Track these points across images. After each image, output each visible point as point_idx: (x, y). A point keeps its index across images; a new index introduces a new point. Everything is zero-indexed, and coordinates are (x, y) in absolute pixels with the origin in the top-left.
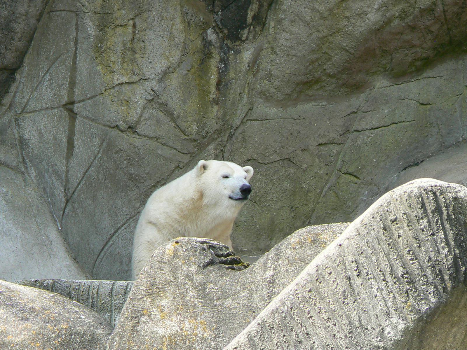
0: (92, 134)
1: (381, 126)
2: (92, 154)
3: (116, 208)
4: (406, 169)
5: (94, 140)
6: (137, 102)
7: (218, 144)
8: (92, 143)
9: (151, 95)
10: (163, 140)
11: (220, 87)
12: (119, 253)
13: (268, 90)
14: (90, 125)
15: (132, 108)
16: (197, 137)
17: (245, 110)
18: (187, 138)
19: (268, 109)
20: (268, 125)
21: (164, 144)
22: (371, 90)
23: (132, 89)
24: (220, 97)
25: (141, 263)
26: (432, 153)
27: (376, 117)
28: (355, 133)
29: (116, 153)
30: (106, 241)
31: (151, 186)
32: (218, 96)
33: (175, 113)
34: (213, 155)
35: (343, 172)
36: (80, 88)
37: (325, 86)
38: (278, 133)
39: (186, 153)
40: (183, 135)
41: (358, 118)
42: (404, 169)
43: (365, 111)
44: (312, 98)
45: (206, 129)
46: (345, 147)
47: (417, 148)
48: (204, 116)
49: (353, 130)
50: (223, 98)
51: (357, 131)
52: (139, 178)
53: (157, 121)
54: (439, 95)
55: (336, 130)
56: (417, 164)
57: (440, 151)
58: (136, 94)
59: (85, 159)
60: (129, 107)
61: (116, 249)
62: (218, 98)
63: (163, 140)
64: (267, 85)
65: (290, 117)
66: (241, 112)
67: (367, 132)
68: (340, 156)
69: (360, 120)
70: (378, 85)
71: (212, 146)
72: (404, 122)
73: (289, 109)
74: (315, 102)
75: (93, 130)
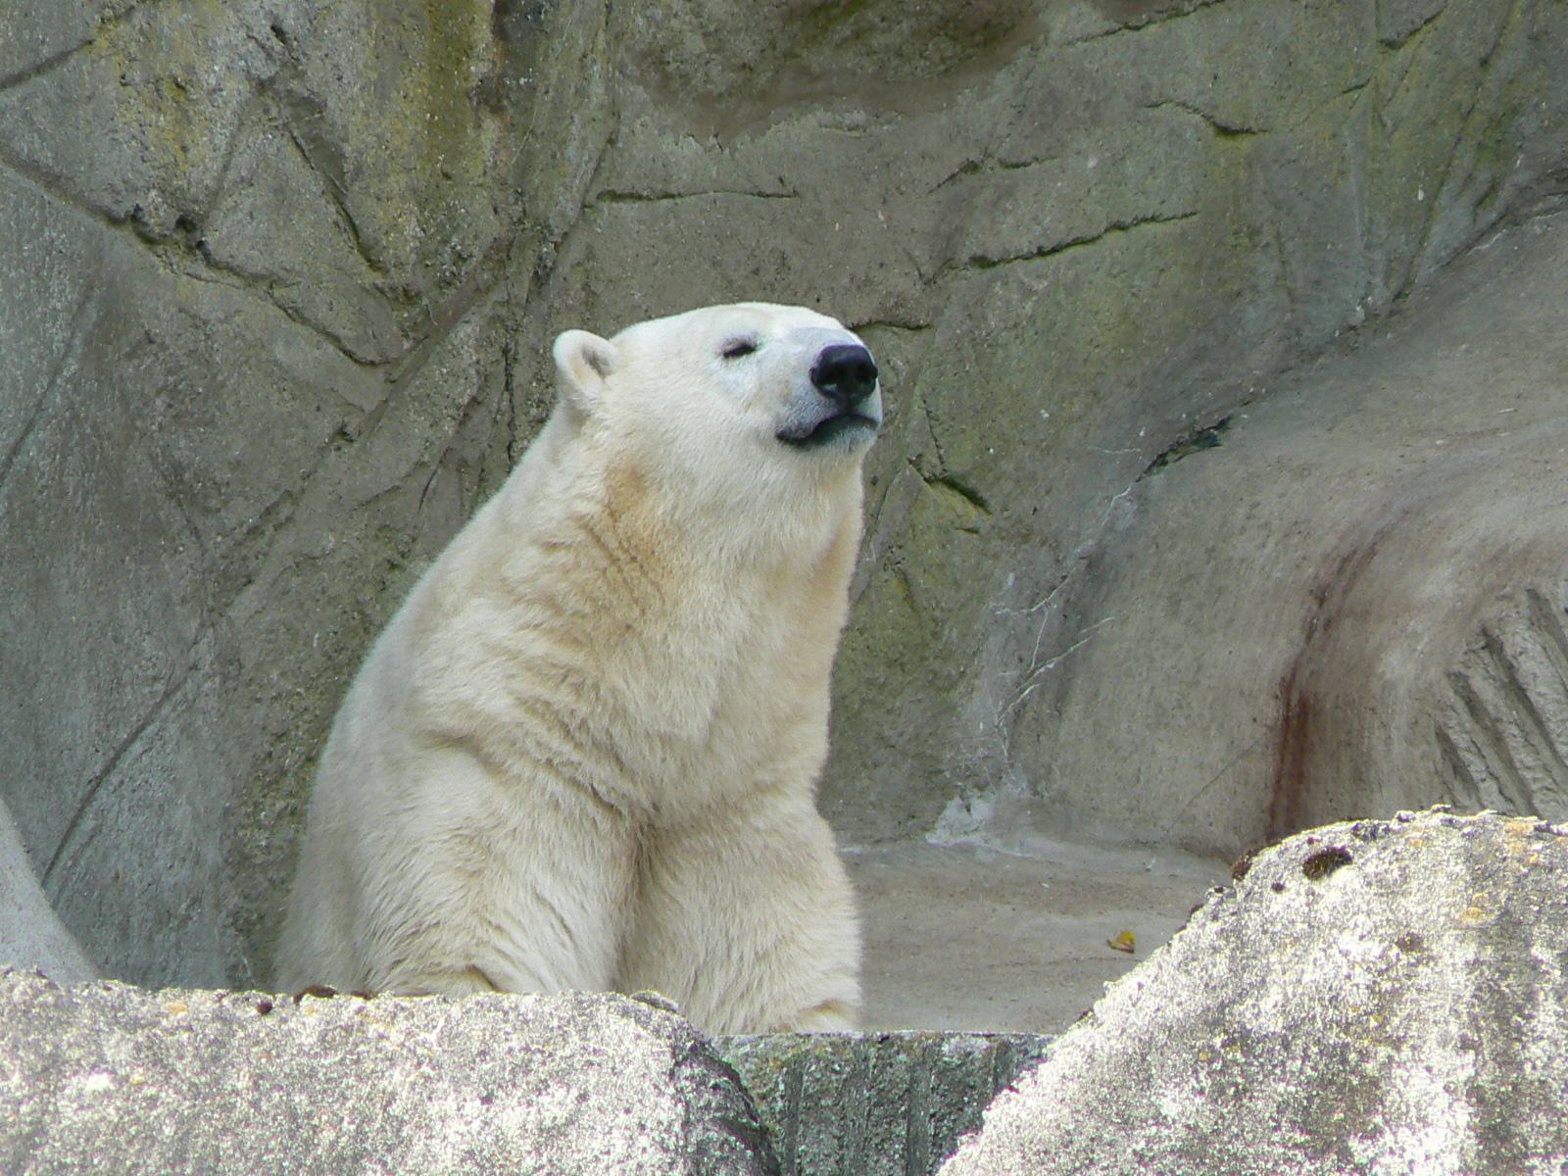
0: (50, 254)
1: (1069, 240)
2: (41, 358)
3: (116, 640)
4: (1165, 463)
5: (55, 288)
6: (214, 91)
7: (496, 319)
8: (47, 301)
9: (269, 56)
10: (294, 293)
11: (510, 20)
12: (117, 877)
13: (676, 42)
14: (42, 207)
15: (195, 119)
16: (421, 281)
17: (595, 143)
18: (380, 282)
19: (669, 138)
20: (672, 225)
21: (295, 314)
22: (1035, 49)
23: (194, 21)
24: (510, 72)
25: (433, 936)
26: (1258, 382)
27: (1054, 194)
28: (974, 273)
29: (129, 356)
30: (71, 815)
31: (245, 529)
32: (498, 71)
33: (347, 149)
34: (472, 372)
35: (927, 475)
36: (16, 13)
37: (872, 28)
38: (707, 266)
39: (372, 363)
40: (364, 268)
41: (988, 194)
42: (1154, 463)
43: (1014, 161)
44: (819, 86)
45: (455, 240)
46: (938, 339)
47: (1200, 354)
48: (448, 168)
49: (966, 258)
50: (522, 81)
51: (982, 262)
52: (204, 486)
53: (276, 192)
54: (1286, 85)
55: (911, 258)
56: (1205, 439)
57: (1283, 372)
58: (210, 49)
59: (15, 381)
60: (184, 119)
61: (105, 857)
62: (501, 77)
63: (294, 293)
64: (676, 15)
65: (748, 186)
66: (578, 154)
67: (1020, 268)
68: (917, 390)
69: (995, 204)
70: (1060, 26)
71: (469, 329)
72: (1153, 219)
73: (742, 142)
74: (827, 111)
75: (54, 235)
